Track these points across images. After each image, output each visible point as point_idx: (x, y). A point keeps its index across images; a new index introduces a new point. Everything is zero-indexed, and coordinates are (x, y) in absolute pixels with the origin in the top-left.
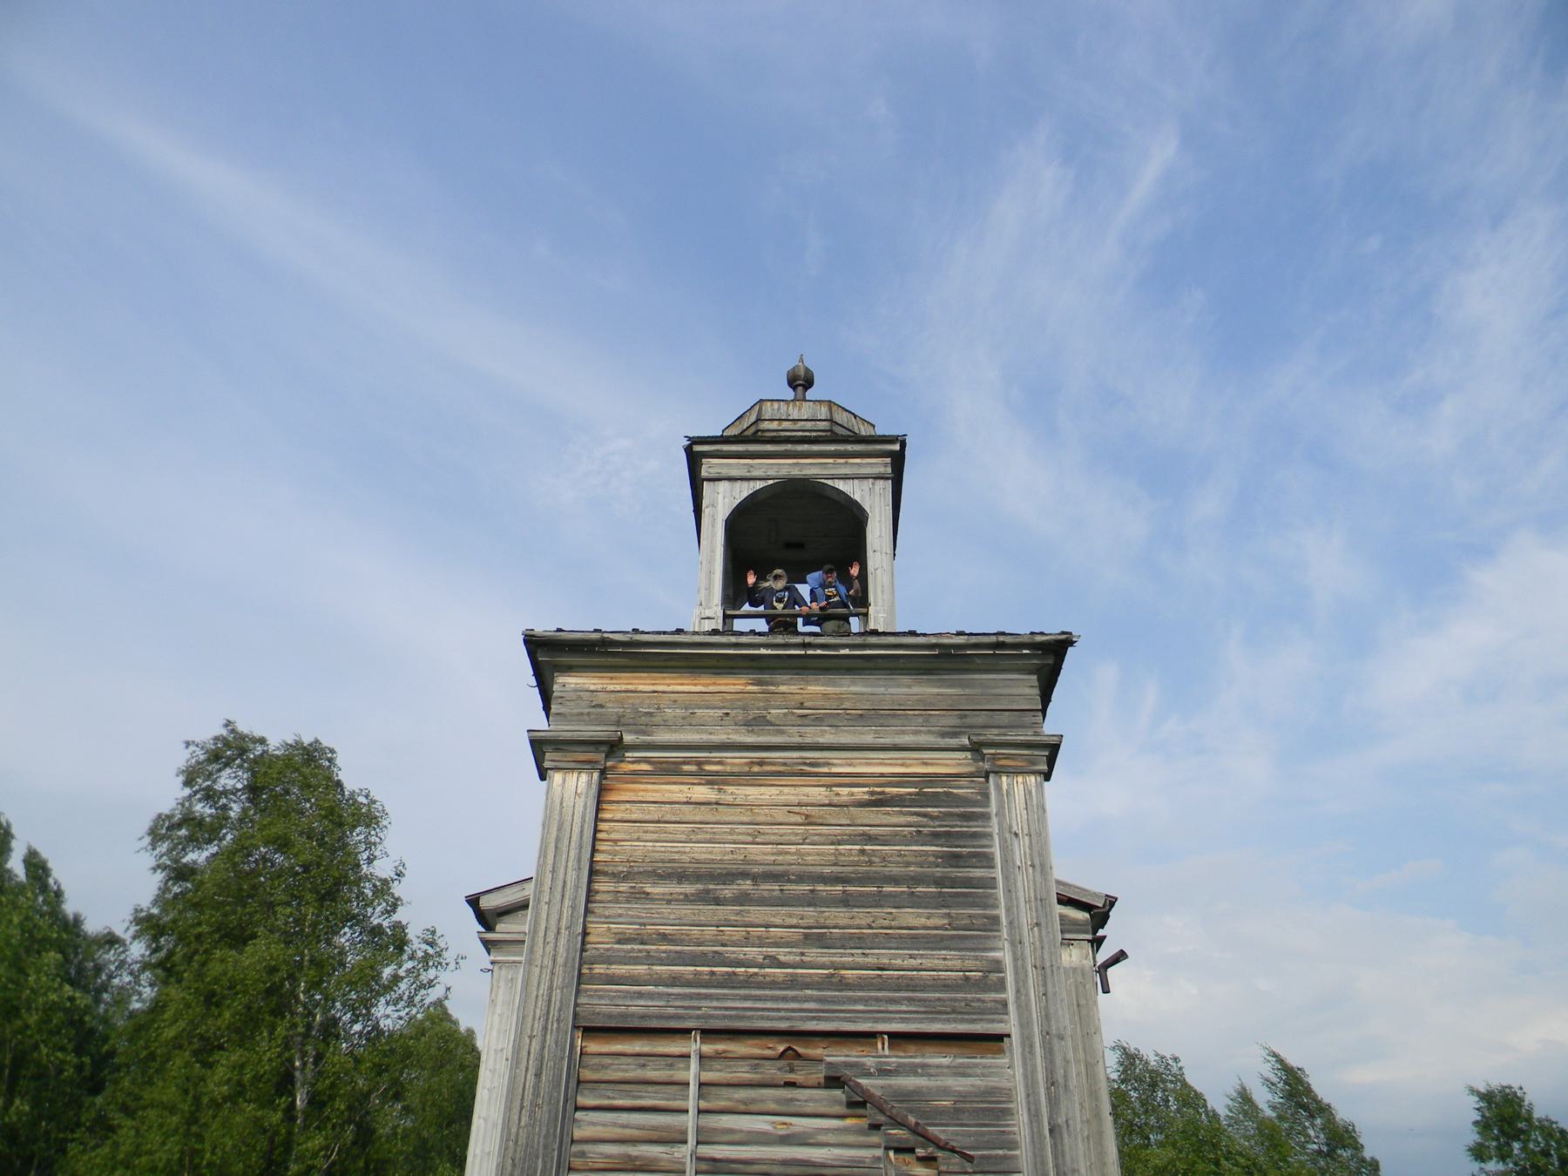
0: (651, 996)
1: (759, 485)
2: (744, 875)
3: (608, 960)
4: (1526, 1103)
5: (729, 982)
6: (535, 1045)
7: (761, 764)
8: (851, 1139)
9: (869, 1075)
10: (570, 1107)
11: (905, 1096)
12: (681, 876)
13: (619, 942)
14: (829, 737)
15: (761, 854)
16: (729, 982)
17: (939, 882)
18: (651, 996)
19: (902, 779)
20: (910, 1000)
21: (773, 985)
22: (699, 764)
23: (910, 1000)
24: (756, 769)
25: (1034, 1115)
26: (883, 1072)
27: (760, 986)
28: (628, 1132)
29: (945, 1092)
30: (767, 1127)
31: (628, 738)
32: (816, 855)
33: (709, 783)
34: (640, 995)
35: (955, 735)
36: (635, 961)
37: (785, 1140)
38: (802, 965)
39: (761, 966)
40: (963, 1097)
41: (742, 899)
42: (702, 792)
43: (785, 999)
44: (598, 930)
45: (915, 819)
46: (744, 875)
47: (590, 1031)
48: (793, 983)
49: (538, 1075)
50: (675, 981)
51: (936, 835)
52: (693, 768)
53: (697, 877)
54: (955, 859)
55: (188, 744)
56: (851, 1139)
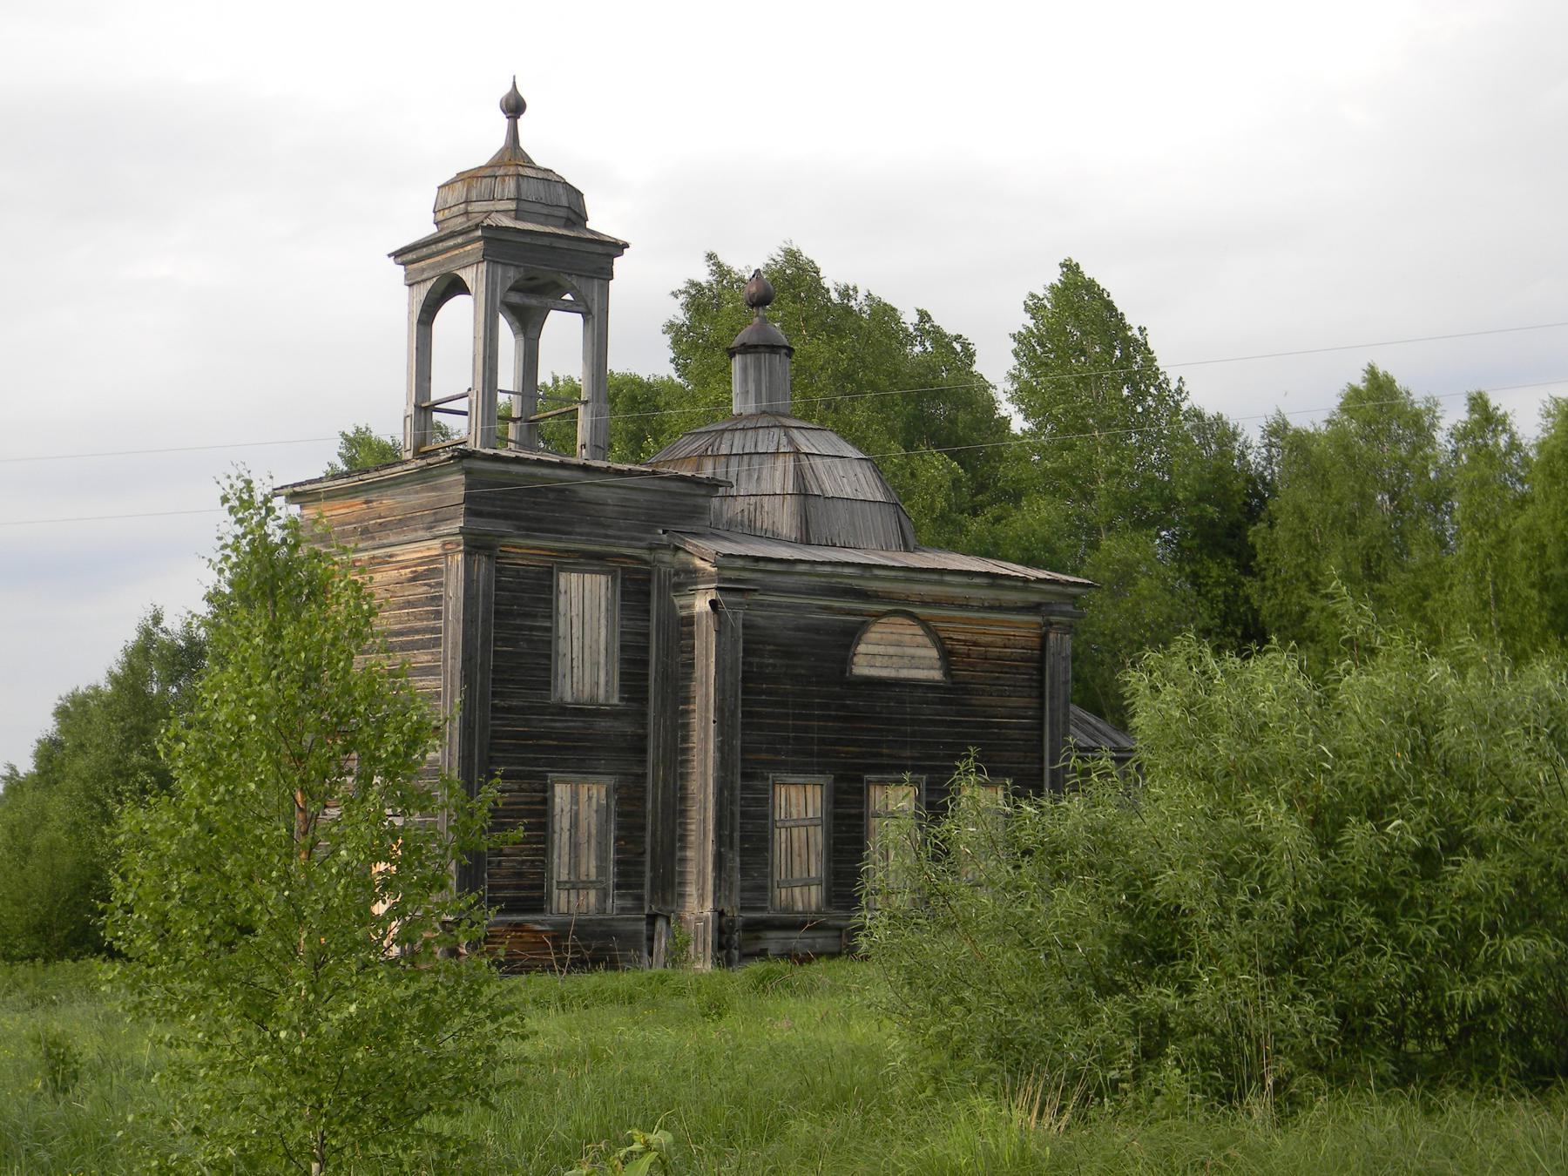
1: (429, 285)
7: (374, 558)
14: (392, 539)
35: (430, 528)
45: (426, 588)
54: (438, 615)
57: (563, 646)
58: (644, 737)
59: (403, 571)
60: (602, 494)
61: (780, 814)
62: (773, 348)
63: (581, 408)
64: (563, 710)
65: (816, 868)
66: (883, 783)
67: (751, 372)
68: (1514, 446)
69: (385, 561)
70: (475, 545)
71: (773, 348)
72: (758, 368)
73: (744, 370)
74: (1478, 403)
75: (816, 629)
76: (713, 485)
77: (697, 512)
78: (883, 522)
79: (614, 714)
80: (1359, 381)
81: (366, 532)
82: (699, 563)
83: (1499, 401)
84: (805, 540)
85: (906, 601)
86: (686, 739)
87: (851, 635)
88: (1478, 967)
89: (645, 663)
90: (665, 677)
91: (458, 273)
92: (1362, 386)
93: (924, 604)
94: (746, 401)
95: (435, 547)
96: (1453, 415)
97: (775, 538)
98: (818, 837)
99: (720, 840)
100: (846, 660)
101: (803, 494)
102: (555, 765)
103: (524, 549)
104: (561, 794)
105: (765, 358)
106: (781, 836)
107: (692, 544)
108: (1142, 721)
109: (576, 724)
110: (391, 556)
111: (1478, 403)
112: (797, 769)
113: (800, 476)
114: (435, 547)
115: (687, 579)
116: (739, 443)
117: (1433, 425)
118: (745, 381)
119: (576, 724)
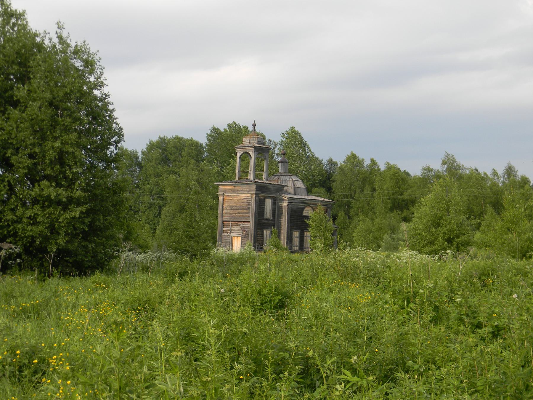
4: (125, 149)
5: (233, 217)
12: (229, 207)
16: (233, 217)
21: (235, 217)
32: (238, 205)
41: (234, 209)
42: (231, 198)
48: (237, 217)
50: (229, 217)
53: (231, 207)
54: (249, 205)
57: (266, 210)
58: (275, 224)
60: (271, 187)
61: (294, 236)
62: (286, 162)
63: (264, 173)
64: (265, 220)
65: (298, 244)
66: (306, 232)
67: (283, 166)
68: (379, 169)
69: (237, 196)
70: (257, 195)
71: (286, 162)
72: (284, 165)
73: (282, 165)
74: (372, 160)
75: (299, 208)
76: (285, 186)
77: (282, 190)
78: (305, 191)
79: (271, 220)
80: (349, 154)
81: (234, 191)
82: (284, 198)
83: (377, 160)
84: (295, 194)
85: (310, 204)
86: (281, 224)
87: (303, 209)
88: (13, 251)
89: (275, 213)
90: (278, 215)
91: (249, 152)
92: (350, 155)
93: (313, 205)
94: (282, 171)
95: (249, 195)
96: (367, 162)
97: (290, 194)
98: (298, 239)
99: (287, 239)
100: (302, 213)
101: (295, 187)
102: (265, 228)
103: (263, 195)
104: (265, 231)
105: (285, 164)
106: (294, 239)
107: (283, 195)
108: (310, 215)
109: (267, 222)
111: (372, 160)
112: (297, 229)
113: (294, 184)
114: (249, 195)
115: (283, 200)
116: (282, 178)
117: (364, 163)
118: (282, 167)
119: (267, 222)
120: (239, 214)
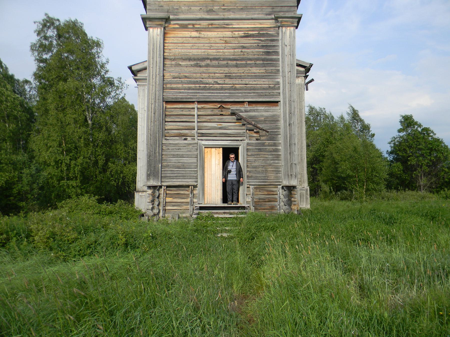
0: (183, 93)
2: (208, 59)
3: (171, 84)
5: (204, 89)
6: (153, 106)
7: (212, 25)
8: (237, 128)
9: (242, 112)
10: (164, 121)
11: (251, 117)
12: (190, 59)
13: (173, 78)
14: (232, 16)
15: (212, 52)
17: (263, 60)
18: (183, 93)
19: (254, 29)
20: (254, 93)
22: (193, 25)
23: (254, 93)
24: (210, 26)
25: (285, 121)
26: (246, 111)
27: (213, 90)
28: (182, 127)
29: (262, 116)
30: (216, 125)
31: (171, 17)
32: (228, 52)
33: (197, 31)
34: (180, 93)
36: (178, 83)
37: (220, 128)
38: (224, 84)
39: (213, 84)
40: (267, 117)
41: (207, 66)
42: (195, 34)
43: (220, 93)
44: (167, 75)
45: (256, 41)
46: (208, 59)
47: (167, 102)
48: (222, 89)
49: (155, 114)
50: (189, 89)
51: (263, 46)
52: (191, 26)
53: (195, 60)
55: (35, 23)
56: (237, 128)
59: (237, 33)
110: (227, 25)
120: (227, 81)
